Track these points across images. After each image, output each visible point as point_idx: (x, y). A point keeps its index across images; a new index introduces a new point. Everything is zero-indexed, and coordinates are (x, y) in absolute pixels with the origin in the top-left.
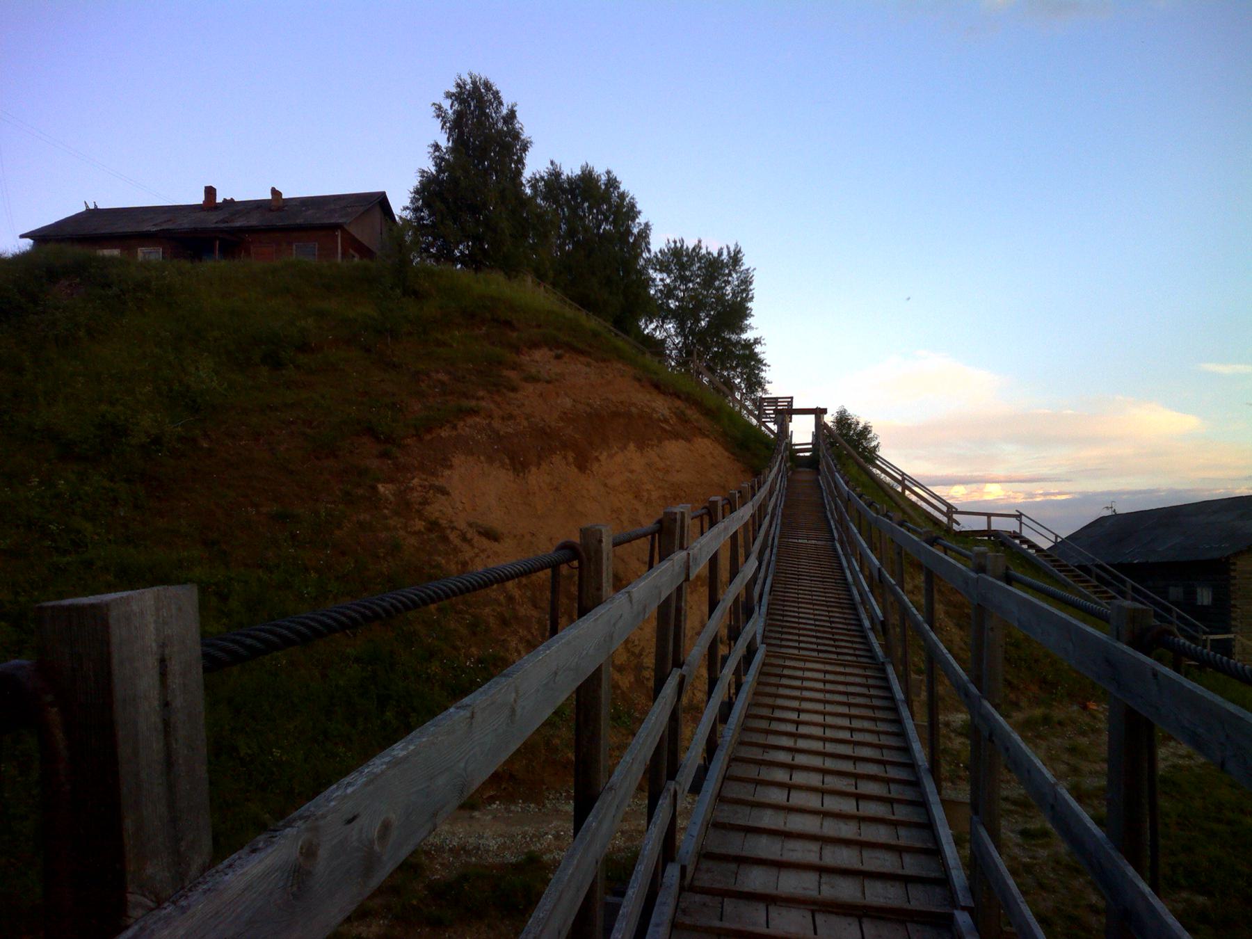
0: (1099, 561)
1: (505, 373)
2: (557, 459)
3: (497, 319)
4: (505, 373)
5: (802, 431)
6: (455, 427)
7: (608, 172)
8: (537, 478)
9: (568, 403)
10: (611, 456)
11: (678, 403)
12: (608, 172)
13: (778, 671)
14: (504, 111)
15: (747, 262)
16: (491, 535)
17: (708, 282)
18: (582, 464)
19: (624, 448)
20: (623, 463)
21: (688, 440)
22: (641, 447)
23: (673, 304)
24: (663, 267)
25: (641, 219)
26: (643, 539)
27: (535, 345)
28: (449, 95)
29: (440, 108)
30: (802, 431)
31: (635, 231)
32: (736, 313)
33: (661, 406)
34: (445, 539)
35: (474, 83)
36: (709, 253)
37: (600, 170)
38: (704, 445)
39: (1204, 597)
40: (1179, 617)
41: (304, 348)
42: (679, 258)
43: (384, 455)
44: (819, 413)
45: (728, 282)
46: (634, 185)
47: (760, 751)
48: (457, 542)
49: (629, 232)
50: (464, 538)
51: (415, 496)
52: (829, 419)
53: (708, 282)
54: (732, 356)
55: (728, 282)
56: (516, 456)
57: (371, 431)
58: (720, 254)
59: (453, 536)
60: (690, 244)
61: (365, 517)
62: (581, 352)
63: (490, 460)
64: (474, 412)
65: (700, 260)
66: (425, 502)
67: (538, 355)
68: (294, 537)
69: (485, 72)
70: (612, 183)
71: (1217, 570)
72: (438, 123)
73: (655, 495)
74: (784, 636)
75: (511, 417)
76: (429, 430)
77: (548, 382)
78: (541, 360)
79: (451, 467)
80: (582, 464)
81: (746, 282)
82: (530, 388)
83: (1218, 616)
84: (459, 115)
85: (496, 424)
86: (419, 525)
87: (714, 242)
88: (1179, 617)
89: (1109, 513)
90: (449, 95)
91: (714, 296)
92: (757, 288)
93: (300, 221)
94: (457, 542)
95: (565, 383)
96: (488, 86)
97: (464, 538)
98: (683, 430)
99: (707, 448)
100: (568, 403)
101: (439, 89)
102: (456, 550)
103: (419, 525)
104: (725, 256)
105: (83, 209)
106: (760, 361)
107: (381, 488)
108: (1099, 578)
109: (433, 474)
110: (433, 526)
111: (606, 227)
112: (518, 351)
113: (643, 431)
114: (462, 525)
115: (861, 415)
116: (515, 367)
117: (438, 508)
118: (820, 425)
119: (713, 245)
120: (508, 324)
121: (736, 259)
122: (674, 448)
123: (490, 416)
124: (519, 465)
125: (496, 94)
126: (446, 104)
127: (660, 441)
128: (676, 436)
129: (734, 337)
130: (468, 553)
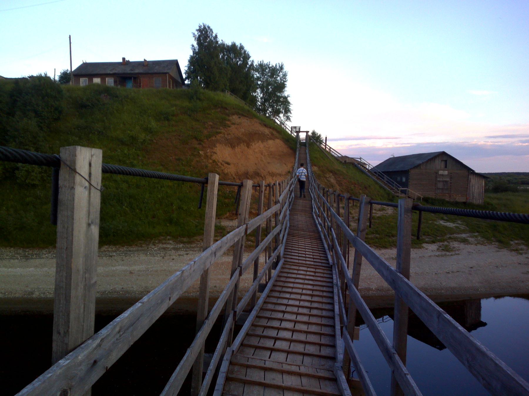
0: (379, 171)
1: (227, 122)
2: (242, 145)
3: (222, 107)
4: (227, 122)
5: (303, 136)
6: (216, 137)
7: (241, 44)
8: (237, 150)
9: (243, 130)
10: (255, 144)
11: (271, 130)
12: (241, 44)
13: (290, 253)
14: (214, 35)
15: (285, 69)
16: (228, 164)
17: (272, 76)
18: (248, 146)
19: (258, 142)
20: (258, 146)
21: (274, 140)
22: (262, 142)
23: (259, 83)
24: (257, 70)
25: (251, 59)
26: (92, 191)
27: (233, 114)
28: (197, 30)
29: (194, 34)
30: (303, 136)
31: (250, 63)
32: (281, 87)
33: (267, 131)
34: (217, 165)
35: (204, 26)
36: (273, 66)
37: (238, 44)
38: (278, 141)
39: (404, 180)
40: (396, 185)
41: (173, 115)
42: (262, 67)
43: (200, 144)
44: (307, 132)
45: (279, 76)
46: (248, 48)
47: (279, 294)
48: (220, 165)
49: (247, 63)
50: (222, 164)
51: (209, 154)
52: (310, 134)
53: (272, 76)
54: (280, 101)
55: (279, 76)
56: (232, 143)
57: (196, 138)
58: (276, 66)
59: (219, 164)
60: (265, 62)
61: (198, 159)
62: (246, 116)
63: (226, 145)
64: (220, 133)
65: (269, 68)
66: (211, 156)
67: (234, 117)
68: (182, 164)
69: (208, 23)
70: (242, 47)
71: (405, 173)
72: (194, 38)
73: (266, 154)
74: (293, 251)
75: (229, 134)
76: (210, 138)
77: (238, 125)
78: (235, 118)
79: (216, 147)
80: (248, 146)
81: (285, 75)
82: (233, 126)
83: (405, 185)
84: (199, 36)
85: (226, 136)
86: (211, 161)
87: (273, 61)
88: (396, 185)
89: (392, 157)
90: (197, 30)
91: (273, 82)
92: (288, 77)
93: (155, 71)
94: (220, 165)
95: (241, 125)
96: (209, 27)
97: (222, 164)
98: (272, 137)
99: (279, 142)
100: (243, 130)
101: (194, 29)
102: (220, 167)
103: (211, 161)
104: (278, 67)
105: (82, 63)
106: (289, 103)
107: (200, 152)
108: (379, 175)
109: (212, 149)
110: (214, 161)
111: (259, 94)
112: (229, 116)
113: (263, 138)
114: (221, 161)
115: (318, 132)
116: (229, 120)
117: (214, 157)
118: (307, 136)
119: (273, 64)
120: (226, 109)
121: (281, 68)
122: (270, 142)
123: (224, 134)
124: (233, 147)
125: (211, 30)
126: (196, 33)
127: (267, 140)
128: (271, 139)
129: (279, 94)
130: (223, 168)
